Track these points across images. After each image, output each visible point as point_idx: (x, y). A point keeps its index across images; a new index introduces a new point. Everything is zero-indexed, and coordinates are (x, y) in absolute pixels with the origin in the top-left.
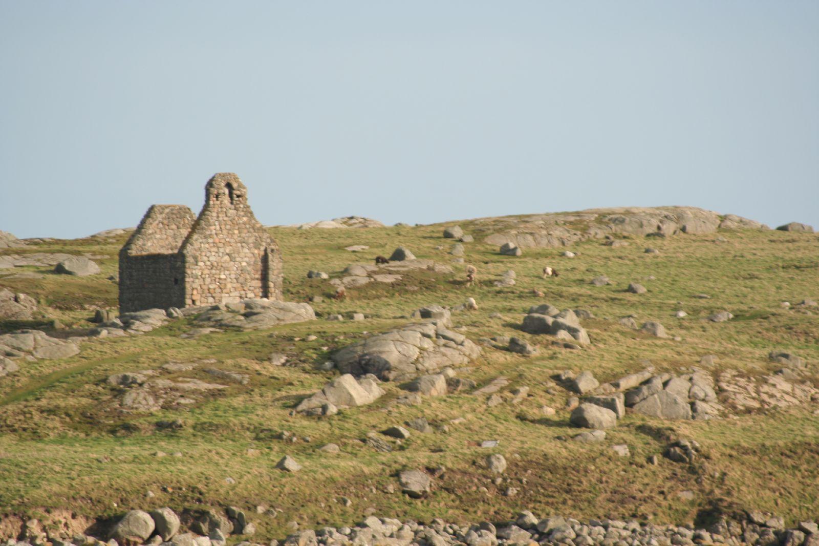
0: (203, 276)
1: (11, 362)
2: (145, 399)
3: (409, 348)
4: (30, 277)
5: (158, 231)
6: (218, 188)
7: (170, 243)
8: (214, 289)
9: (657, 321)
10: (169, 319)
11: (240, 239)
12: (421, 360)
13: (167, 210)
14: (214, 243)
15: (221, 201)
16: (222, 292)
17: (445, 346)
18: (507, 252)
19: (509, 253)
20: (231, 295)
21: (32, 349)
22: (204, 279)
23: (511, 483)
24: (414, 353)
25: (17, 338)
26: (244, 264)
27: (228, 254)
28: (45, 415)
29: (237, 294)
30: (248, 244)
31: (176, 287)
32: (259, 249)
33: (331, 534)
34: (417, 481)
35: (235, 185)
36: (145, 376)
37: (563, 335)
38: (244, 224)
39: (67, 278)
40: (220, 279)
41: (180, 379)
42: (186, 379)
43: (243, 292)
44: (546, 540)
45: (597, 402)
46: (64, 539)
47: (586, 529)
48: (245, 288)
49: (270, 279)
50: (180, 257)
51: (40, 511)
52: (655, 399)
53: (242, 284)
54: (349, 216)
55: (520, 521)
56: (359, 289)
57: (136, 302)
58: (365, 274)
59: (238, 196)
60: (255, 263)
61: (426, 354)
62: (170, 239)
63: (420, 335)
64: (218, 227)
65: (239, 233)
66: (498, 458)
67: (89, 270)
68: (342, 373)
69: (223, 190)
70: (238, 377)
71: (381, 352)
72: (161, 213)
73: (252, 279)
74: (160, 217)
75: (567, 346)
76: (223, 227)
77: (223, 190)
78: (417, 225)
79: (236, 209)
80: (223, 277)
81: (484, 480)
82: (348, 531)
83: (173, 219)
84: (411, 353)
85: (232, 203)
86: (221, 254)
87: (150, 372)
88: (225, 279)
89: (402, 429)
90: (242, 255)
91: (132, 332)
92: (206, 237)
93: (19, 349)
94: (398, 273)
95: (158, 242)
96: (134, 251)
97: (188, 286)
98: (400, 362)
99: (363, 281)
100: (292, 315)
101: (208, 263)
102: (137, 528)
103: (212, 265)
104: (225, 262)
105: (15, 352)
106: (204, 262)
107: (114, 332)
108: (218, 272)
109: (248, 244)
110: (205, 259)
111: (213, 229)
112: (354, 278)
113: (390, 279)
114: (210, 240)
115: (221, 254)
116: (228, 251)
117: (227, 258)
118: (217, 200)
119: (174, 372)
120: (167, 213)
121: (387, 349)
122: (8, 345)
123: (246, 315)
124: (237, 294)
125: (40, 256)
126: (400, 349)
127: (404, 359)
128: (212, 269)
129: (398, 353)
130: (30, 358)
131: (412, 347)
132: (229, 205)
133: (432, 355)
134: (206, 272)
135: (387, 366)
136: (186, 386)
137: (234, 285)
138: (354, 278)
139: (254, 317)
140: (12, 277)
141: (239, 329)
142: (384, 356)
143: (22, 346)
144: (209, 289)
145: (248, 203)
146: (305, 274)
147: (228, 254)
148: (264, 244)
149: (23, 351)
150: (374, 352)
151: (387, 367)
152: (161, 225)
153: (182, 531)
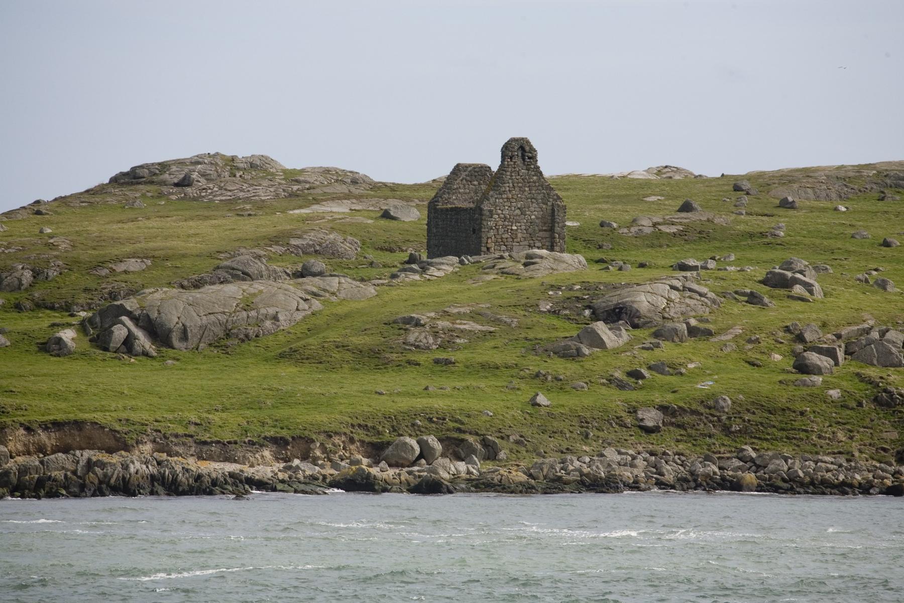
5: (462, 186)
7: (472, 198)
9: (582, 346)
12: (667, 309)
13: (469, 169)
17: (690, 298)
18: (785, 204)
22: (498, 229)
24: (663, 303)
26: (533, 217)
33: (572, 461)
34: (651, 417)
35: (527, 149)
36: (428, 317)
37: (798, 289)
38: (534, 182)
39: (393, 224)
45: (820, 351)
46: (342, 460)
51: (322, 437)
55: (741, 455)
56: (646, 237)
59: (529, 158)
60: (543, 217)
61: (672, 304)
63: (668, 287)
69: (519, 152)
70: (508, 320)
71: (633, 302)
73: (540, 231)
74: (464, 175)
75: (802, 299)
77: (519, 152)
78: (723, 175)
82: (587, 459)
85: (524, 164)
87: (432, 314)
89: (644, 371)
90: (532, 209)
92: (500, 194)
93: (325, 290)
95: (460, 200)
96: (440, 206)
98: (649, 311)
99: (648, 230)
100: (564, 265)
102: (405, 453)
103: (505, 217)
104: (517, 215)
110: (500, 212)
113: (673, 229)
117: (518, 212)
119: (454, 314)
121: (638, 299)
123: (525, 265)
130: (333, 299)
131: (660, 298)
132: (521, 165)
133: (677, 305)
134: (500, 223)
136: (462, 327)
139: (532, 267)
142: (635, 306)
143: (328, 288)
144: (502, 238)
145: (539, 164)
146: (598, 223)
150: (627, 302)
152: (464, 181)
153: (443, 455)
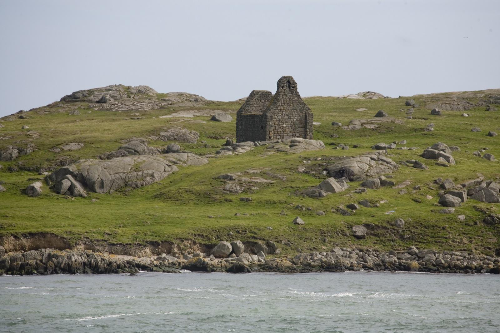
0: (275, 125)
1: (175, 167)
2: (235, 187)
3: (364, 165)
4: (199, 122)
5: (255, 103)
6: (283, 84)
8: (280, 132)
10: (255, 147)
11: (293, 108)
12: (369, 171)
13: (260, 93)
14: (280, 109)
15: (285, 90)
16: (284, 133)
17: (382, 164)
18: (434, 113)
19: (436, 114)
20: (288, 134)
21: (186, 160)
22: (275, 127)
23: (406, 232)
25: (179, 155)
27: (287, 115)
28: (188, 193)
29: (291, 134)
30: (297, 110)
31: (262, 130)
32: (302, 113)
33: (316, 255)
36: (237, 175)
37: (441, 160)
38: (296, 101)
40: (283, 127)
41: (253, 177)
42: (256, 178)
43: (294, 133)
44: (422, 260)
45: (454, 194)
47: (441, 255)
48: (295, 132)
49: (307, 128)
50: (265, 116)
52: (482, 192)
53: (293, 129)
54: (367, 91)
57: (244, 137)
58: (360, 124)
59: (293, 87)
62: (261, 107)
63: (370, 159)
64: (283, 102)
65: (293, 105)
66: (401, 220)
67: (229, 119)
68: (331, 177)
69: (287, 84)
70: (281, 177)
71: (350, 167)
72: (257, 95)
75: (444, 165)
76: (285, 102)
77: (287, 84)
79: (292, 94)
80: (284, 126)
81: (393, 231)
83: (263, 97)
84: (365, 168)
85: (290, 91)
86: (284, 115)
87: (239, 174)
88: (286, 127)
89: (356, 205)
90: (294, 115)
91: (237, 153)
92: (277, 107)
93: (180, 160)
94: (376, 123)
96: (243, 114)
97: (267, 130)
98: (359, 172)
99: (358, 127)
100: (312, 147)
101: (278, 119)
104: (286, 119)
105: (178, 162)
106: (276, 119)
107: (227, 153)
108: (282, 123)
109: (297, 110)
110: (276, 117)
111: (280, 103)
112: (354, 126)
113: (372, 127)
114: (279, 108)
115: (284, 115)
116: (287, 114)
117: (286, 117)
118: (283, 89)
120: (260, 94)
121: (353, 165)
122: (175, 158)
123: (291, 146)
124: (291, 134)
125: (207, 111)
126: (359, 166)
127: (361, 170)
128: (279, 122)
129: (358, 167)
130: (184, 165)
131: (365, 165)
132: (289, 91)
134: (277, 123)
135: (353, 173)
136: (256, 181)
137: (290, 130)
138: (354, 126)
139: (294, 147)
140: (190, 122)
141: (286, 153)
142: (351, 169)
143: (181, 159)
144: (278, 132)
147: (287, 115)
148: (305, 110)
149: (182, 161)
150: (346, 167)
151: (352, 173)
153: (245, 251)
